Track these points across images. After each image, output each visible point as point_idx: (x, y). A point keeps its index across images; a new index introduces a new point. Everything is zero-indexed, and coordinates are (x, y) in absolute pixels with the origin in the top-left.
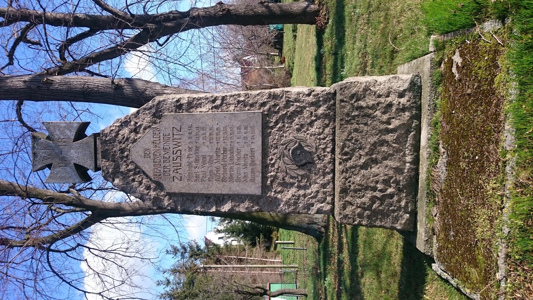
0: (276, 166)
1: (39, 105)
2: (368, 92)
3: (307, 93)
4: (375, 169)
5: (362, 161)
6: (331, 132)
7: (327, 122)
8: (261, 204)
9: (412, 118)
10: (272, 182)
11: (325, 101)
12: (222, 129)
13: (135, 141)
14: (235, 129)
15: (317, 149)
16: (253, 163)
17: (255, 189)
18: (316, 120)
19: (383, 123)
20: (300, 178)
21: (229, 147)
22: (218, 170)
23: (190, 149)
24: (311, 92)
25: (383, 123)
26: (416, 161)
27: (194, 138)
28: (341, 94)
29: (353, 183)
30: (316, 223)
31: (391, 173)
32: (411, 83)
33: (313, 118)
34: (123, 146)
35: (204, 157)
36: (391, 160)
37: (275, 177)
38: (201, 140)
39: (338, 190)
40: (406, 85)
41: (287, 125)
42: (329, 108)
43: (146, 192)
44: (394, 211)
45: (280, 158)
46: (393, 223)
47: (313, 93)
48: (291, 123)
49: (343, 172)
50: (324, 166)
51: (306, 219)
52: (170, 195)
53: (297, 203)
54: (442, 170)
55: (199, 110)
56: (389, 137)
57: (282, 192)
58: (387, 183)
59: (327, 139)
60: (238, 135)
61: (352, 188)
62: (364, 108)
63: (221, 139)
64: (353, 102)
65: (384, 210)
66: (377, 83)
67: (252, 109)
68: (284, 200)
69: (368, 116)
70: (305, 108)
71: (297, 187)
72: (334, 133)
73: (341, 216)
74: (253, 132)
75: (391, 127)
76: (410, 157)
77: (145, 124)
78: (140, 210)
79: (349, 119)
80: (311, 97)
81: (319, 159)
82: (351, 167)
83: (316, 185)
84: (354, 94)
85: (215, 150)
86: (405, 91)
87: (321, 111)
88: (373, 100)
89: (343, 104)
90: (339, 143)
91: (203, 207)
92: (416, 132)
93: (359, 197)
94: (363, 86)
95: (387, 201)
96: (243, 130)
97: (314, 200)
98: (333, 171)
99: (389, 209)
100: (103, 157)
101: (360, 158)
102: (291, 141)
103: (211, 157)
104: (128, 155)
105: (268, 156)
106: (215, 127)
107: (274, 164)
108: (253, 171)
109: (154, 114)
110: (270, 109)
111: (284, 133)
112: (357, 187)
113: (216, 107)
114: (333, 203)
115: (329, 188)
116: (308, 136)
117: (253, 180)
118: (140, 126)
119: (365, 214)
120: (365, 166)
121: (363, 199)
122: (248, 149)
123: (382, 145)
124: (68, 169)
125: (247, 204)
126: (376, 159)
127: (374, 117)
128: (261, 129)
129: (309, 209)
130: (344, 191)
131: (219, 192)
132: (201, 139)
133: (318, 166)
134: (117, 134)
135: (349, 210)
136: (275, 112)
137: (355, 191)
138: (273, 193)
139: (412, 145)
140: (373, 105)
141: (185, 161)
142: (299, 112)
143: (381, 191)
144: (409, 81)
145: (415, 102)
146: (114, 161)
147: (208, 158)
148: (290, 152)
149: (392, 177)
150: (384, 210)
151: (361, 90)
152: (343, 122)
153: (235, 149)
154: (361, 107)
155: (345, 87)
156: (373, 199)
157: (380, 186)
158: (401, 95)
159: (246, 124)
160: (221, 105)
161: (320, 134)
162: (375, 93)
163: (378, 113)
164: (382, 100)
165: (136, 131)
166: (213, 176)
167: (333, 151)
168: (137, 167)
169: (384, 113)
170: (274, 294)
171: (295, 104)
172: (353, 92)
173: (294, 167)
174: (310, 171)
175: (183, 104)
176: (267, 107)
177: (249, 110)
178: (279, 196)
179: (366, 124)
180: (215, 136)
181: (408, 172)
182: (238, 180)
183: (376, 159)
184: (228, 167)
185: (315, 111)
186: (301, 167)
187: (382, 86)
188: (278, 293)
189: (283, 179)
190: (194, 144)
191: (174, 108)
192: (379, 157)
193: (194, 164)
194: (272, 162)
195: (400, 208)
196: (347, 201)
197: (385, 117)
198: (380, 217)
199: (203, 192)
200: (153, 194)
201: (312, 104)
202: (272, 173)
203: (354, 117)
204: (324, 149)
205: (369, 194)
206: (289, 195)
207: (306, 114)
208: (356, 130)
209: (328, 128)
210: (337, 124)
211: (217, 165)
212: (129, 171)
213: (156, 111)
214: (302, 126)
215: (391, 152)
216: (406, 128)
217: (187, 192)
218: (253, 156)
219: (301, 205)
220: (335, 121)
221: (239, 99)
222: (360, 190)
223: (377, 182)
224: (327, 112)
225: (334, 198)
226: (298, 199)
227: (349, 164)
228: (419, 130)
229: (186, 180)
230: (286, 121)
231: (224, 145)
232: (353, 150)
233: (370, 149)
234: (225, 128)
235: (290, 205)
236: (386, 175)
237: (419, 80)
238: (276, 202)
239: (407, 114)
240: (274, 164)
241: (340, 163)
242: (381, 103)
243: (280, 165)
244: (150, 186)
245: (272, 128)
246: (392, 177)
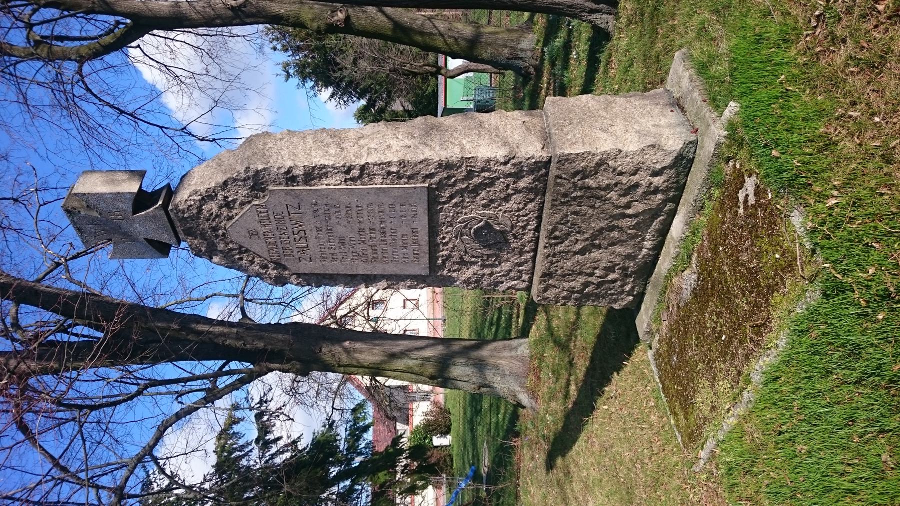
0: (450, 245)
2: (603, 167)
3: (502, 161)
4: (595, 254)
6: (537, 208)
7: (531, 196)
10: (444, 262)
11: (531, 172)
12: (365, 206)
14: (386, 207)
15: (512, 227)
16: (416, 243)
18: (514, 194)
19: (618, 207)
20: (485, 257)
22: (364, 250)
24: (509, 160)
25: (618, 207)
26: (658, 247)
28: (558, 168)
29: (562, 268)
30: (521, 58)
32: (676, 158)
33: (510, 191)
34: (214, 224)
35: (341, 238)
36: (621, 245)
37: (449, 256)
40: (669, 160)
41: (467, 200)
47: (513, 161)
48: (475, 197)
51: (506, 51)
54: (688, 280)
55: (325, 181)
56: (624, 223)
58: (610, 269)
59: (530, 216)
60: (391, 214)
61: (559, 272)
62: (593, 189)
63: (366, 218)
64: (576, 179)
66: (621, 155)
67: (411, 181)
68: (462, 279)
70: (498, 178)
72: (541, 210)
75: (629, 211)
76: (650, 242)
77: (240, 199)
78: (216, 18)
79: (563, 200)
80: (509, 165)
83: (508, 264)
85: (357, 230)
87: (522, 184)
88: (608, 178)
89: (559, 180)
92: (668, 217)
94: (597, 159)
96: (398, 208)
98: (535, 251)
101: (576, 243)
104: (224, 235)
105: (438, 235)
111: (462, 208)
112: (566, 272)
113: (353, 179)
116: (501, 213)
117: (417, 261)
118: (234, 201)
120: (582, 252)
121: (573, 284)
128: (426, 207)
130: (547, 275)
131: (369, 273)
132: (333, 218)
134: (200, 210)
137: (563, 276)
138: (445, 272)
139: (657, 231)
140: (608, 185)
141: (312, 242)
144: (674, 155)
145: (677, 182)
148: (472, 231)
151: (593, 164)
152: (555, 203)
153: (387, 230)
154: (589, 188)
155: (567, 160)
156: (586, 284)
158: (656, 174)
161: (519, 210)
163: (612, 194)
164: (624, 179)
166: (360, 257)
167: (537, 229)
168: (240, 247)
170: (452, 74)
171: (483, 174)
172: (579, 168)
175: (298, 176)
176: (436, 179)
177: (406, 183)
178: (455, 275)
181: (643, 258)
184: (379, 248)
185: (514, 183)
187: (628, 159)
188: (458, 72)
190: (324, 223)
194: (444, 241)
197: (624, 200)
201: (510, 175)
202: (444, 253)
203: (575, 199)
204: (524, 228)
205: (582, 279)
207: (499, 186)
209: (533, 204)
213: (255, 184)
219: (485, 283)
220: (544, 195)
221: (388, 169)
223: (596, 268)
224: (533, 185)
225: (532, 277)
227: (559, 248)
228: (672, 214)
230: (466, 195)
237: (693, 149)
239: (659, 196)
241: (545, 247)
242: (622, 184)
243: (456, 243)
245: (444, 203)
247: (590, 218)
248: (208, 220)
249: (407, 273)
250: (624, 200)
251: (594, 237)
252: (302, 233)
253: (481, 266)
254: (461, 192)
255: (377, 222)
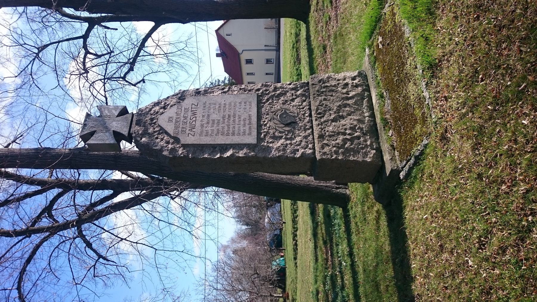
0: (268, 125)
1: (86, 28)
4: (343, 122)
5: (332, 117)
7: (304, 98)
8: (256, 151)
9: (364, 90)
10: (265, 136)
11: (302, 87)
13: (163, 113)
14: (237, 104)
17: (252, 140)
18: (296, 98)
19: (344, 94)
20: (286, 133)
21: (232, 114)
23: (203, 116)
25: (344, 94)
26: (373, 116)
27: (207, 110)
31: (355, 123)
33: (294, 97)
35: (213, 121)
36: (354, 115)
37: (268, 133)
38: (212, 110)
39: (316, 136)
42: (305, 91)
43: (165, 145)
44: (362, 148)
45: (270, 121)
46: (364, 157)
48: (278, 100)
49: (319, 125)
50: (305, 125)
52: (184, 146)
53: (285, 150)
56: (350, 102)
57: (273, 142)
58: (353, 129)
61: (327, 134)
65: (355, 148)
68: (275, 147)
69: (333, 91)
71: (285, 138)
72: (310, 105)
73: (321, 153)
74: (250, 105)
77: (172, 103)
81: (300, 120)
82: (325, 121)
84: (321, 80)
86: (355, 76)
87: (299, 93)
90: (313, 108)
91: (209, 155)
93: (333, 140)
95: (356, 141)
97: (298, 147)
98: (312, 127)
99: (358, 147)
100: (137, 124)
101: (330, 116)
102: (279, 110)
103: (219, 120)
104: (155, 122)
106: (223, 102)
107: (266, 124)
108: (250, 128)
109: (180, 97)
110: (263, 92)
112: (331, 133)
114: (314, 148)
115: (310, 138)
117: (250, 134)
118: (168, 105)
119: (340, 152)
122: (247, 115)
123: (345, 107)
124: (107, 134)
125: (245, 151)
126: (342, 115)
127: (336, 91)
129: (295, 154)
131: (224, 143)
133: (300, 125)
135: (326, 149)
136: (267, 94)
137: (330, 136)
142: (284, 94)
143: (349, 134)
146: (145, 126)
147: (216, 121)
149: (356, 125)
150: (355, 148)
153: (237, 115)
154: (327, 86)
156: (345, 141)
157: (348, 132)
159: (245, 101)
160: (228, 91)
162: (335, 79)
164: (341, 82)
165: (164, 108)
167: (310, 115)
168: (162, 128)
169: (343, 88)
172: (320, 79)
173: (283, 126)
174: (294, 128)
176: (261, 91)
178: (271, 145)
179: (332, 96)
180: (222, 108)
181: (368, 122)
182: (239, 134)
183: (342, 115)
186: (287, 125)
189: (274, 133)
191: (194, 94)
192: (345, 114)
193: (205, 125)
195: (367, 146)
196: (324, 144)
197: (344, 91)
198: (352, 153)
199: (211, 143)
200: (170, 146)
201: (292, 89)
203: (322, 92)
204: (304, 115)
205: (341, 137)
206: (279, 144)
207: (288, 94)
208: (325, 99)
210: (311, 99)
211: (223, 125)
212: (155, 132)
213: (181, 96)
214: (286, 101)
215: (353, 110)
216: (361, 96)
217: (198, 143)
218: (250, 119)
219: (288, 151)
220: (310, 98)
222: (333, 136)
223: (346, 129)
226: (286, 147)
227: (322, 120)
229: (198, 135)
231: (228, 113)
232: (325, 111)
233: (337, 110)
234: (230, 104)
235: (280, 150)
236: (352, 124)
238: (268, 149)
239: (359, 88)
240: (266, 124)
241: (316, 120)
244: (169, 141)
245: (264, 103)
246: (356, 125)
247: (333, 101)
248: (152, 115)
249: (244, 142)
250: (344, 91)
251: (338, 111)
252: (195, 118)
253: (285, 138)
254: (272, 97)
255: (232, 112)
